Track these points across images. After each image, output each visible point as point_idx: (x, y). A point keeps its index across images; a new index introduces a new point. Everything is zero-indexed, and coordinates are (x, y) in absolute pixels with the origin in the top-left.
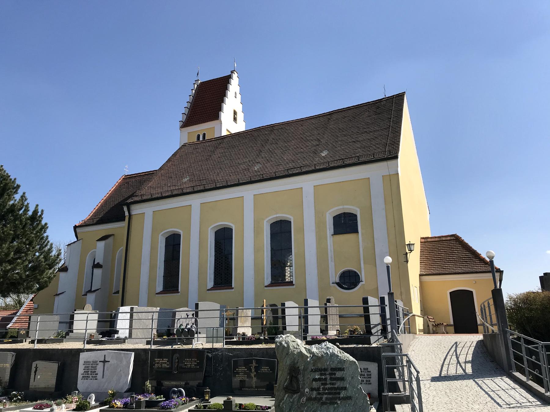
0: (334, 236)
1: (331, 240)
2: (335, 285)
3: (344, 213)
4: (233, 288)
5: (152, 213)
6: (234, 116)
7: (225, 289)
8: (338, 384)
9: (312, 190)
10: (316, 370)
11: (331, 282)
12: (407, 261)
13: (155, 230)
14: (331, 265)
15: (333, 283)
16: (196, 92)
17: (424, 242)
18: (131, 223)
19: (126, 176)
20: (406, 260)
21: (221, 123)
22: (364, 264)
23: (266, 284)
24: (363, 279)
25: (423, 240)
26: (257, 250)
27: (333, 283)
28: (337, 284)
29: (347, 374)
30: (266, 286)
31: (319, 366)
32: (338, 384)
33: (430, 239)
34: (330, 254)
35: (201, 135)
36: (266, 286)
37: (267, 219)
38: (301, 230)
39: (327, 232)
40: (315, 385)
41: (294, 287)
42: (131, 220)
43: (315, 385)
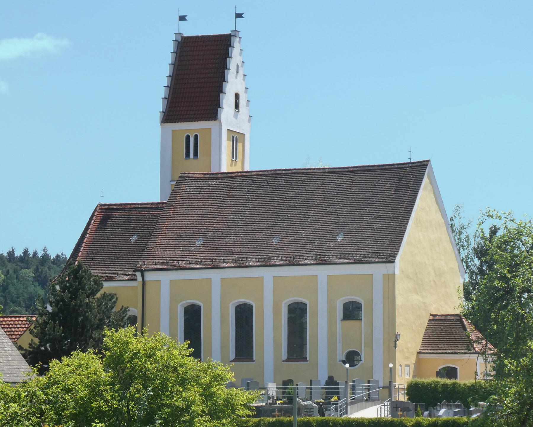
0: (343, 321)
1: (339, 324)
2: (341, 363)
3: (352, 301)
4: (254, 361)
5: (169, 282)
6: (236, 101)
7: (247, 361)
8: (312, 413)
9: (325, 279)
10: (305, 409)
11: (338, 360)
12: (396, 347)
13: (173, 301)
14: (339, 346)
15: (340, 361)
16: (178, 54)
17: (433, 320)
18: (145, 289)
19: (102, 205)
20: (395, 346)
21: (220, 124)
22: (364, 347)
23: (284, 359)
24: (363, 358)
25: (431, 318)
26: (276, 328)
27: (340, 361)
28: (343, 362)
29: (314, 410)
30: (283, 361)
31: (307, 408)
32: (312, 413)
33: (440, 317)
34: (339, 337)
35: (192, 137)
36: (283, 361)
37: (286, 301)
38: (315, 314)
39: (336, 317)
40: (305, 413)
41: (308, 362)
42: (145, 286)
43: (305, 413)
